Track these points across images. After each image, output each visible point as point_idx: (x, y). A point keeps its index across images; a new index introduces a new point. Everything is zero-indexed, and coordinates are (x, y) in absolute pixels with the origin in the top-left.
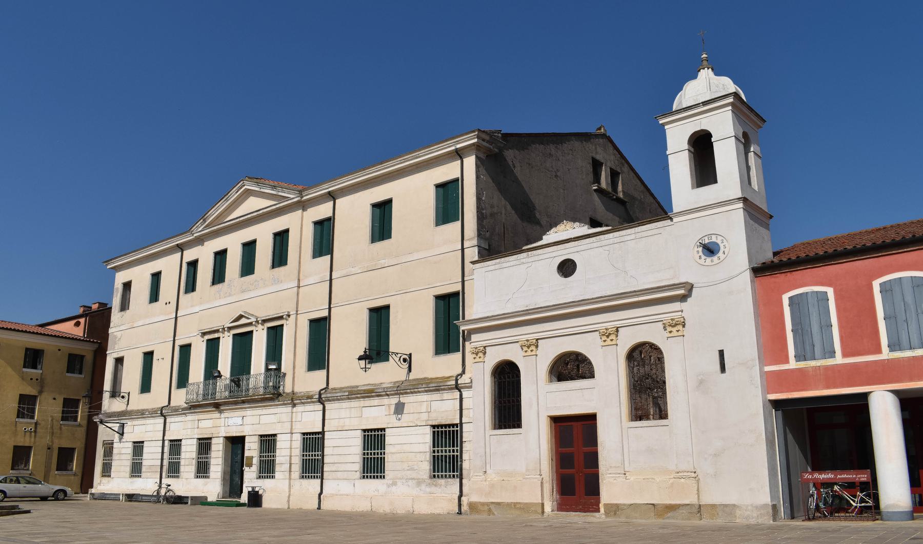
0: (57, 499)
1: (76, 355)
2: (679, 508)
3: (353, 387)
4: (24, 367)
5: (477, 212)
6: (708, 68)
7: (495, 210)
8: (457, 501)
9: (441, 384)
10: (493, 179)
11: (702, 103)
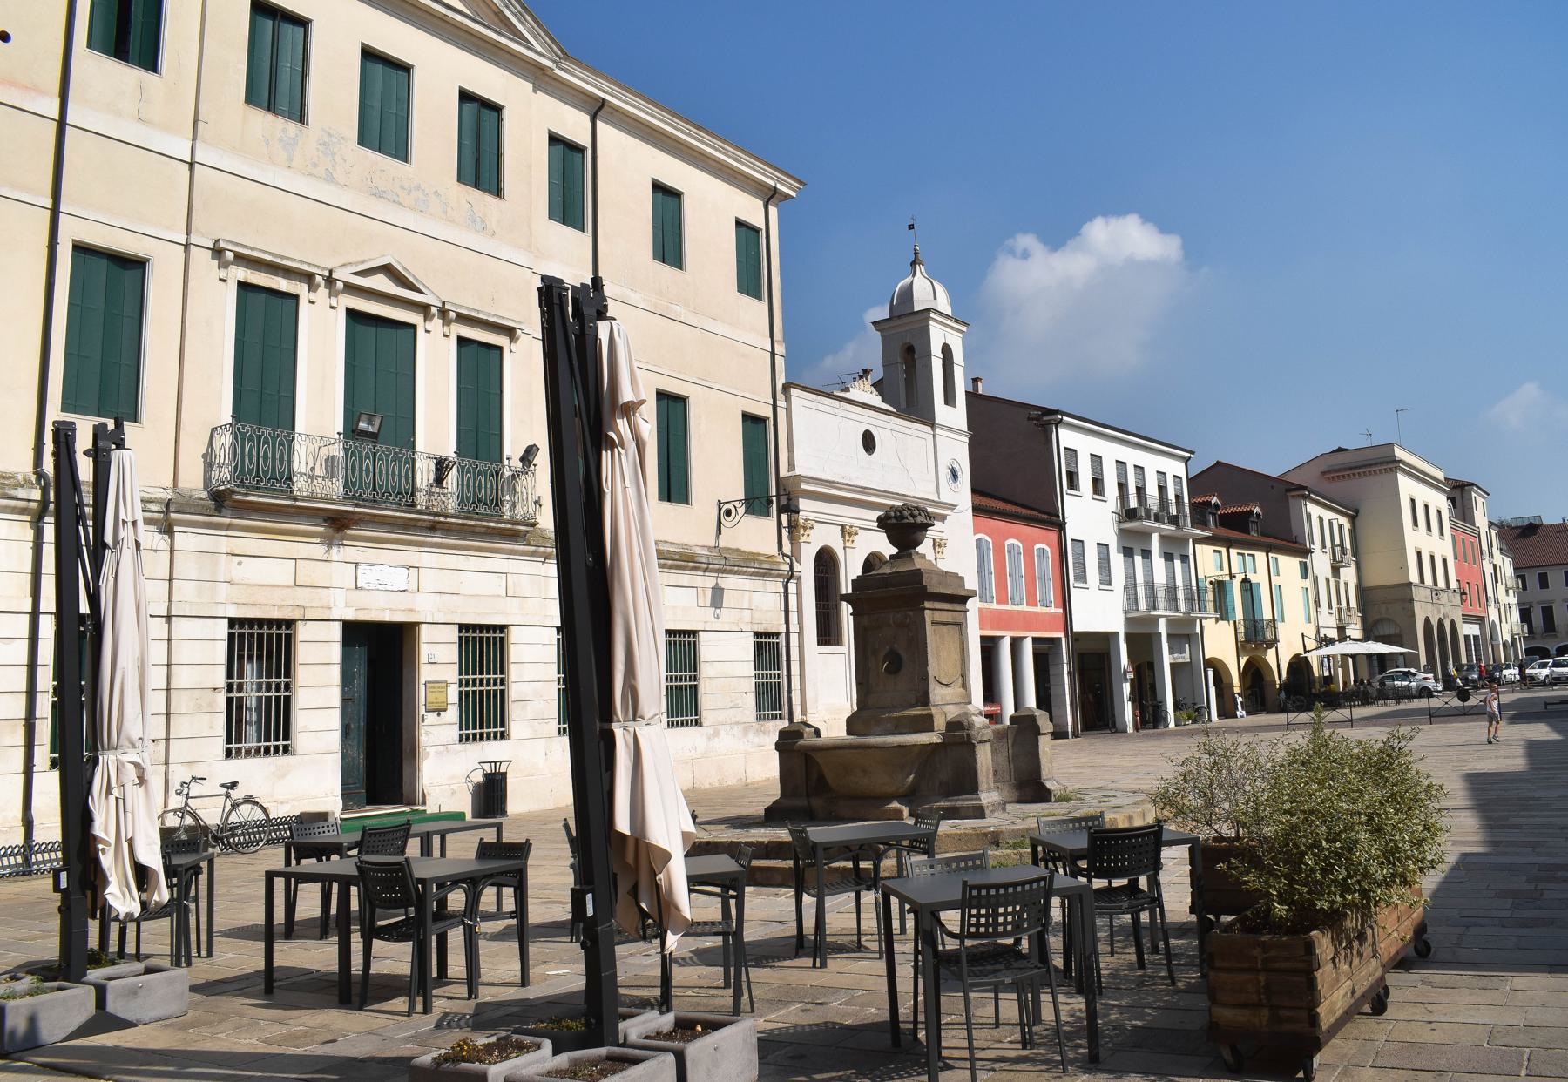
9: (775, 567)
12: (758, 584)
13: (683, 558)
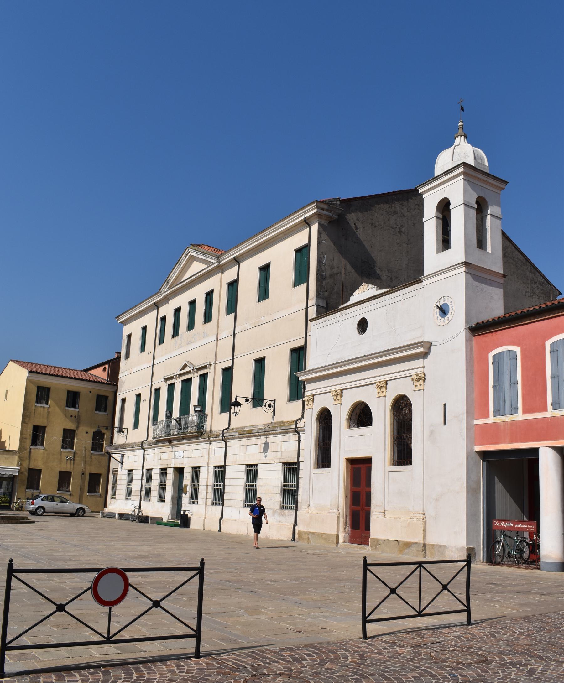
0: (79, 516)
1: (102, 396)
2: (411, 545)
3: (242, 428)
4: (67, 406)
5: (317, 274)
6: (461, 136)
7: (335, 271)
8: (292, 529)
9: (288, 428)
10: (334, 244)
11: (444, 173)
12: (285, 437)
13: (248, 432)
